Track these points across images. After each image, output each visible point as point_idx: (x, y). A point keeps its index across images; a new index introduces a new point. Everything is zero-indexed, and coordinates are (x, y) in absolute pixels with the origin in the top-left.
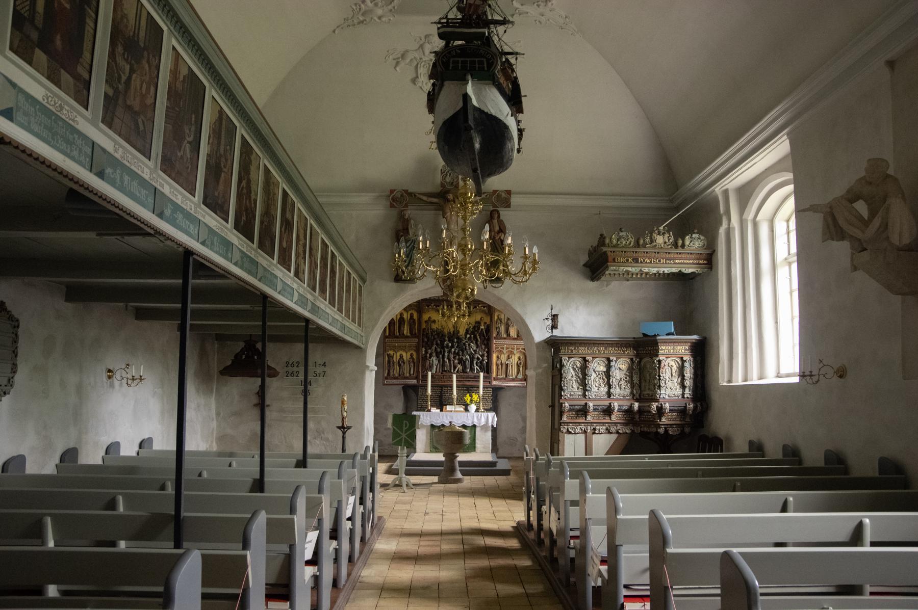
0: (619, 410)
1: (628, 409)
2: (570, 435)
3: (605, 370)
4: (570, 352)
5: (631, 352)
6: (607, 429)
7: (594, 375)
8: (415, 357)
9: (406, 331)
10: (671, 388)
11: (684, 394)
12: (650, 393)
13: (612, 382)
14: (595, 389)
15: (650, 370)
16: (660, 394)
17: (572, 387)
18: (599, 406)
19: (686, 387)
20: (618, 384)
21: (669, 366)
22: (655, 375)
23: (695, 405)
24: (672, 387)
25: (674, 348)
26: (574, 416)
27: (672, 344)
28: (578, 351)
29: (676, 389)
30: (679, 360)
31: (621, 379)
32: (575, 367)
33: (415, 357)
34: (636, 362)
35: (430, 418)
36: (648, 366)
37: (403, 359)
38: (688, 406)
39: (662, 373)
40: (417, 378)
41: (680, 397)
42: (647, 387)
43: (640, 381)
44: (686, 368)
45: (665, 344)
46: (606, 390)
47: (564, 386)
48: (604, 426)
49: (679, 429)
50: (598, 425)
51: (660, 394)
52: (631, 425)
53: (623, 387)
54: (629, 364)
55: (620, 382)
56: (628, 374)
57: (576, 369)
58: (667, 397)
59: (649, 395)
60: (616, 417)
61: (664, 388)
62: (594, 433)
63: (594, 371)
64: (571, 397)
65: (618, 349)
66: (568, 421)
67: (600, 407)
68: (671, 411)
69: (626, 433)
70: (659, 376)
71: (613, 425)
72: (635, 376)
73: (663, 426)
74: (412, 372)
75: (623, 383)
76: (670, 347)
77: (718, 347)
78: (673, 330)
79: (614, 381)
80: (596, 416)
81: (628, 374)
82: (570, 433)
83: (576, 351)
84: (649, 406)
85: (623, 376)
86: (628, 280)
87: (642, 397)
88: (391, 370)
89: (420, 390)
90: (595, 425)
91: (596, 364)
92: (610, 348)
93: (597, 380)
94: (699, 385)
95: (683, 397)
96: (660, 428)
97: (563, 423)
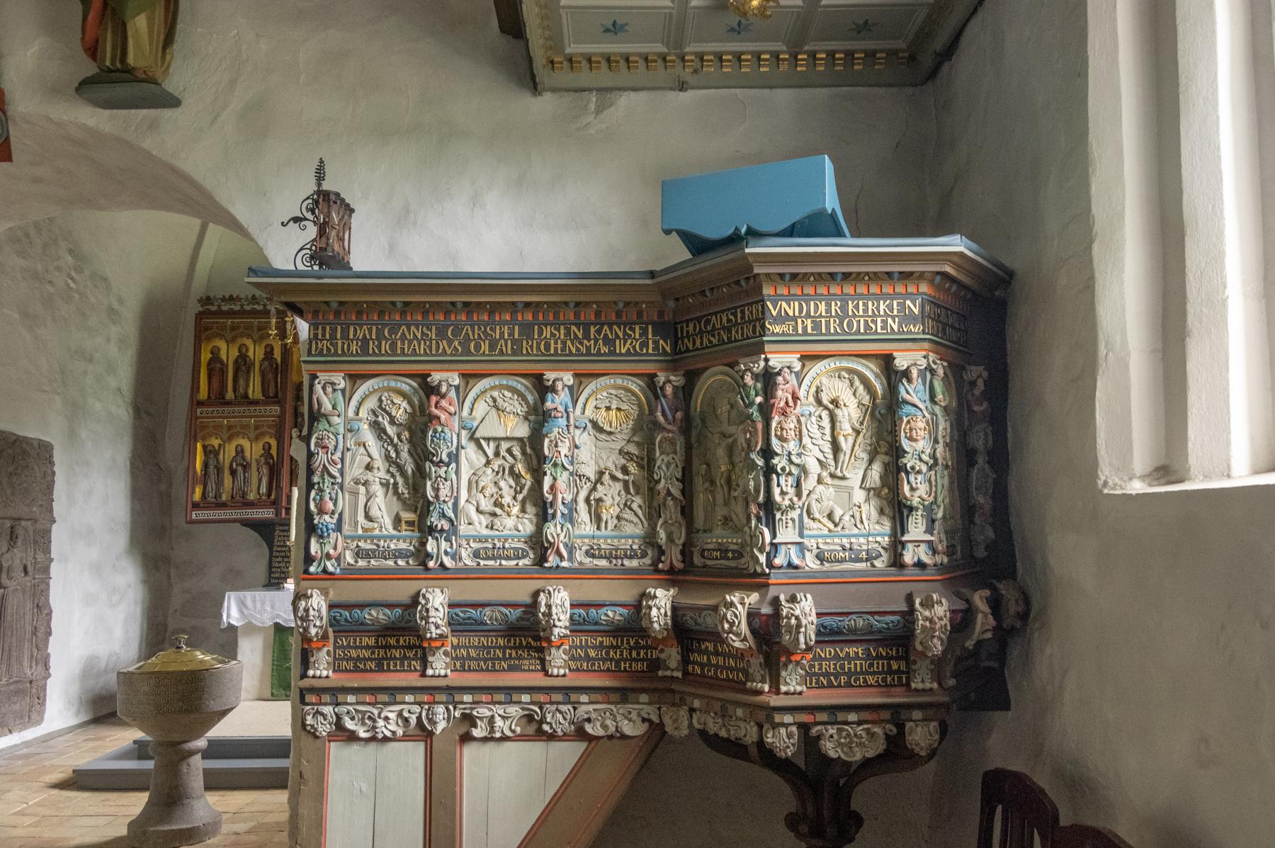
0: (577, 625)
1: (628, 620)
2: (353, 752)
3: (523, 431)
5: (644, 345)
6: (529, 718)
7: (470, 457)
8: (274, 452)
9: (255, 390)
10: (830, 516)
11: (903, 544)
12: (732, 541)
13: (552, 487)
14: (474, 524)
15: (732, 429)
16: (775, 546)
17: (368, 517)
18: (484, 605)
19: (911, 509)
20: (587, 500)
21: (819, 402)
22: (750, 449)
23: (961, 605)
24: (838, 513)
25: (844, 308)
26: (367, 654)
27: (835, 289)
28: (393, 346)
29: (858, 521)
30: (870, 370)
31: (601, 473)
32: (385, 423)
33: (274, 452)
34: (669, 390)
35: (272, 607)
36: (723, 408)
37: (243, 458)
38: (922, 613)
39: (782, 439)
40: (275, 504)
41: (879, 564)
42: (721, 512)
43: (686, 479)
44: (907, 409)
45: (795, 290)
46: (528, 527)
47: (321, 512)
48: (511, 702)
49: (877, 730)
50: (484, 698)
51: (775, 546)
52: (644, 698)
53: (610, 512)
54: (640, 405)
55: (594, 489)
56: (633, 449)
57: (391, 430)
58: (811, 563)
59: (724, 551)
60: (573, 658)
61: (795, 514)
62: (466, 738)
63: (472, 438)
64: (362, 563)
65: (587, 336)
66: (337, 680)
67: (488, 611)
68: (827, 635)
69: (624, 737)
70: (768, 453)
71: (558, 697)
72: (660, 459)
73: (788, 719)
74: (264, 490)
75: (611, 494)
76: (822, 307)
77: (1088, 287)
78: (831, 201)
79: (560, 485)
80: (473, 653)
81: (633, 449)
82: (352, 737)
83: (385, 346)
84: (715, 608)
85: (612, 462)
86: (683, 87)
87: (697, 560)
88: (211, 485)
89: (277, 533)
90: (467, 698)
91: (482, 408)
92: (547, 332)
93: (487, 478)
94: (981, 500)
95: (897, 562)
96: (775, 726)
97: (312, 690)
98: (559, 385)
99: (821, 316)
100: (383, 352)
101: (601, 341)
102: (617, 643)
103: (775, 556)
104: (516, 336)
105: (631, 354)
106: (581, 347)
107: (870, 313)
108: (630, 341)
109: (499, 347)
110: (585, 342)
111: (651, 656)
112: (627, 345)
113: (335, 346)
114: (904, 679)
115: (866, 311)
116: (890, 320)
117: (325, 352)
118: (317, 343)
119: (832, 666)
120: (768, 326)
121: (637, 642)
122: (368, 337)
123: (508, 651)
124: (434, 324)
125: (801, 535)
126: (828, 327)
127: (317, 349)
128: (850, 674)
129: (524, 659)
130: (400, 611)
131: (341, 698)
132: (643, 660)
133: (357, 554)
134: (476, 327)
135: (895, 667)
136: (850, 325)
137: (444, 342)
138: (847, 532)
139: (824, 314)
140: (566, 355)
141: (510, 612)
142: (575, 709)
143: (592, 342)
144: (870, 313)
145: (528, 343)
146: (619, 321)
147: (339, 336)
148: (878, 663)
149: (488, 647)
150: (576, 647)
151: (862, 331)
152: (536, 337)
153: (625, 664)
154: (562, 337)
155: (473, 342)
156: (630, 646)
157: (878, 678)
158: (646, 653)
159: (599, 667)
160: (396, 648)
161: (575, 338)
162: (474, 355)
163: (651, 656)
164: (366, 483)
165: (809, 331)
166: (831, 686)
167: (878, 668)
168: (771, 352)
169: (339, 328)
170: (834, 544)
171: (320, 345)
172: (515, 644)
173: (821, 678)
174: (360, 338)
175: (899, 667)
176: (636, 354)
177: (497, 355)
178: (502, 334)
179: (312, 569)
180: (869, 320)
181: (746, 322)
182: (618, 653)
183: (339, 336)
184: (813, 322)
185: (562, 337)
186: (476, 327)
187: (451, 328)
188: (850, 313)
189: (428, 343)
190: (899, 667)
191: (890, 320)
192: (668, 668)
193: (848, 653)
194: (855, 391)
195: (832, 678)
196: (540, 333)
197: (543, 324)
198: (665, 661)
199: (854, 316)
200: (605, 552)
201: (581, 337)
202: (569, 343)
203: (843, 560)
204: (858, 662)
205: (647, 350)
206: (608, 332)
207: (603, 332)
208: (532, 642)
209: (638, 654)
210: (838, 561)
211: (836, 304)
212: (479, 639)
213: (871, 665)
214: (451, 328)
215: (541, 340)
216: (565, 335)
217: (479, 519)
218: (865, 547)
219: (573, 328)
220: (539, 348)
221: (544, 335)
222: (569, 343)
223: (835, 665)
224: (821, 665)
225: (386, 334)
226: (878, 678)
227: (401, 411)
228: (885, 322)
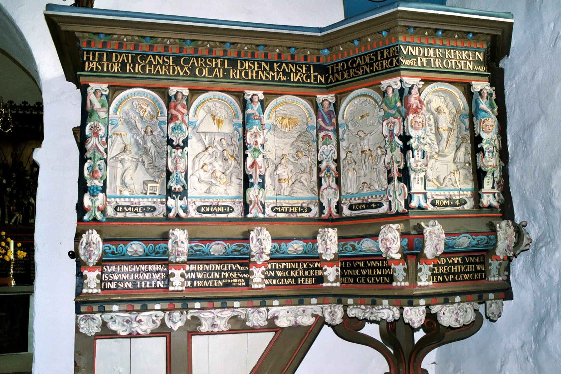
4: (116, 68)
5: (308, 77)
17: (124, 183)
28: (144, 68)
52: (314, 300)
60: (267, 278)
64: (120, 215)
65: (272, 69)
76: (431, 51)
80: (199, 276)
82: (114, 335)
92: (246, 65)
98: (256, 99)
99: (431, 57)
100: (137, 71)
101: (281, 73)
102: (295, 266)
103: (410, 202)
104: (226, 66)
105: (300, 83)
106: (268, 76)
107: (458, 58)
108: (299, 74)
109: (215, 73)
110: (271, 73)
111: (317, 274)
112: (298, 77)
113: (102, 66)
114: (483, 275)
115: (455, 56)
116: (468, 63)
117: (95, 70)
118: (89, 64)
119: (445, 269)
120: (402, 60)
121: (308, 265)
122: (126, 61)
123: (223, 273)
124: (171, 56)
125: (425, 188)
126: (435, 64)
127: (88, 68)
128: (454, 274)
129: (234, 278)
130: (152, 245)
131: (107, 308)
132: (312, 277)
133: (116, 209)
134: (199, 59)
135: (479, 268)
136: (447, 63)
137: (179, 68)
138: (447, 188)
139: (432, 56)
140: (259, 80)
141: (228, 246)
142: (268, 310)
143: (276, 73)
144: (458, 58)
145: (233, 71)
146: (293, 61)
147: (105, 60)
148: (470, 267)
149: (209, 271)
150: (269, 270)
151: (454, 67)
152: (239, 68)
153: (301, 280)
154: (256, 69)
155: (198, 69)
156: (304, 268)
157: (470, 275)
158: (314, 273)
159: (284, 282)
160: (146, 273)
161: (264, 70)
162: (198, 77)
163: (317, 274)
164: (122, 161)
165: (425, 65)
166: (444, 281)
167: (470, 269)
168: (404, 76)
169: (105, 54)
170: (441, 195)
171: (91, 65)
172: (228, 268)
173: (439, 277)
174: (120, 61)
175: (481, 268)
176: (303, 82)
177: (214, 78)
178: (217, 65)
179: (86, 218)
180: (458, 61)
181: (384, 59)
182: (296, 273)
183: (105, 60)
184: (427, 60)
185: (256, 69)
186: (199, 59)
187: (183, 58)
188: (447, 57)
189: (167, 67)
190: (481, 268)
191: (468, 63)
192: (328, 282)
193: (453, 261)
194: (448, 104)
195: (445, 276)
196: (242, 65)
197: (244, 60)
198: (327, 276)
199: (449, 58)
200: (285, 209)
201: (268, 69)
202: (260, 73)
203: (446, 206)
204: (459, 266)
205: (310, 80)
206: (286, 68)
207: (283, 68)
208: (239, 267)
209: (309, 273)
210: (443, 206)
211: (439, 51)
212: (203, 266)
213: (466, 268)
214: (183, 58)
215: (243, 70)
216: (258, 68)
217: (410, 84)
218: (458, 198)
219: (263, 64)
220: (241, 75)
221: (244, 67)
222: (260, 73)
223: (446, 268)
224: (438, 269)
225: (139, 60)
226: (470, 275)
227: (146, 113)
228: (465, 63)
